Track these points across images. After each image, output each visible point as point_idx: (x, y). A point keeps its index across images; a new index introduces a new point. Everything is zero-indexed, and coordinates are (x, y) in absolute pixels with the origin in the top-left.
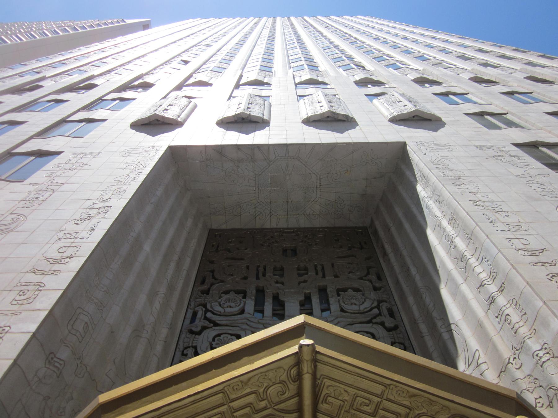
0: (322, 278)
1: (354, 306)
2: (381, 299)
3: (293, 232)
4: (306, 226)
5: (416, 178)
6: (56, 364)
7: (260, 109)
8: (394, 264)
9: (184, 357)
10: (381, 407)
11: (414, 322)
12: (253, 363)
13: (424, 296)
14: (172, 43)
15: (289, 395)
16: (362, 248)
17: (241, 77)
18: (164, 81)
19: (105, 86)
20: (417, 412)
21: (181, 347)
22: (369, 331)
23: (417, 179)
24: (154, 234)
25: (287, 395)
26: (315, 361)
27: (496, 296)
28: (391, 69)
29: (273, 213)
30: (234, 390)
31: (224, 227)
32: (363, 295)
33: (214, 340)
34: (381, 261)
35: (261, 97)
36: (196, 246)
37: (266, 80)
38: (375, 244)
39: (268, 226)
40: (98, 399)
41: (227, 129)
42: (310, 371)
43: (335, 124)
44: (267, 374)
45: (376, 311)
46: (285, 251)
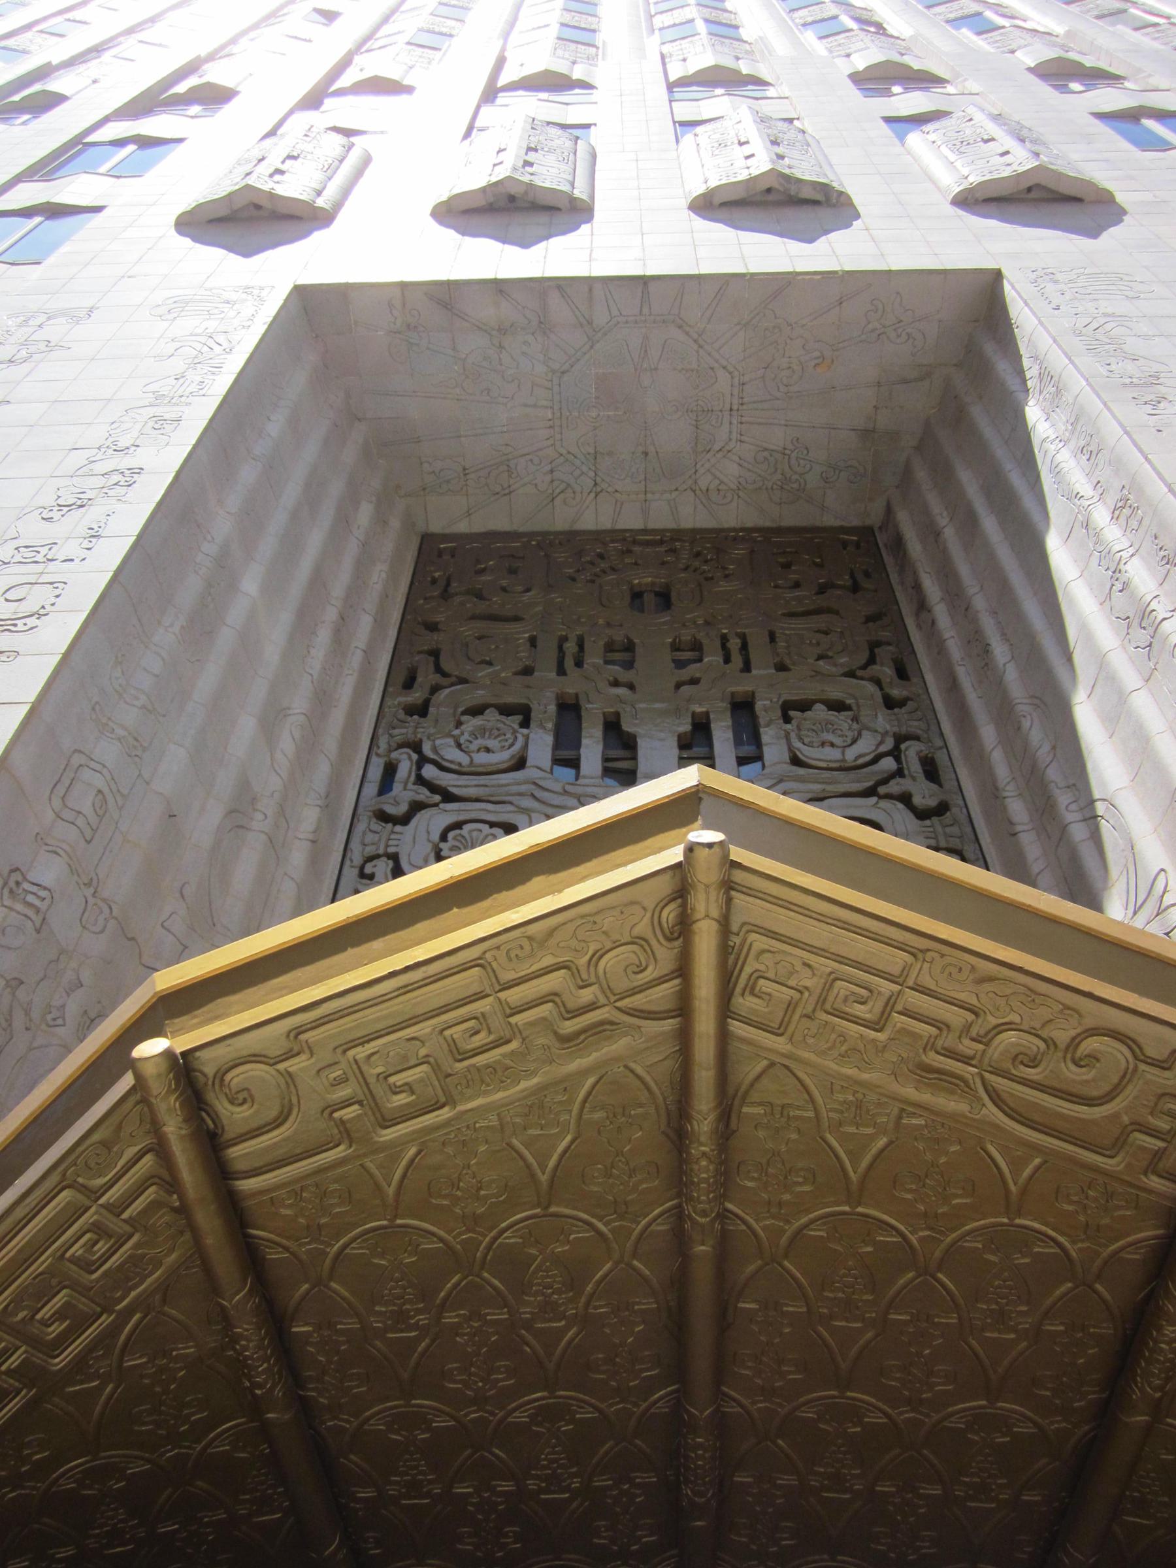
0: (742, 671)
1: (828, 749)
2: (904, 730)
3: (661, 542)
4: (698, 525)
5: (1024, 381)
6: (30, 898)
7: (563, 167)
8: (946, 635)
9: (365, 881)
10: (899, 1007)
11: (993, 795)
12: (560, 891)
13: (1026, 724)
14: (256, 26)
15: (656, 974)
16: (855, 588)
17: (500, 62)
18: (263, 80)
19: (90, 96)
20: (994, 1021)
21: (357, 857)
22: (868, 816)
23: (1029, 384)
24: (268, 546)
25: (650, 974)
26: (728, 886)
28: (966, 33)
29: (604, 486)
30: (510, 960)
31: (462, 527)
32: (855, 719)
33: (444, 837)
34: (910, 623)
35: (564, 127)
36: (386, 582)
37: (577, 74)
38: (894, 578)
39: (588, 523)
40: (154, 982)
41: (464, 234)
42: (715, 913)
43: (790, 212)
44: (597, 919)
45: (888, 764)
46: (637, 596)
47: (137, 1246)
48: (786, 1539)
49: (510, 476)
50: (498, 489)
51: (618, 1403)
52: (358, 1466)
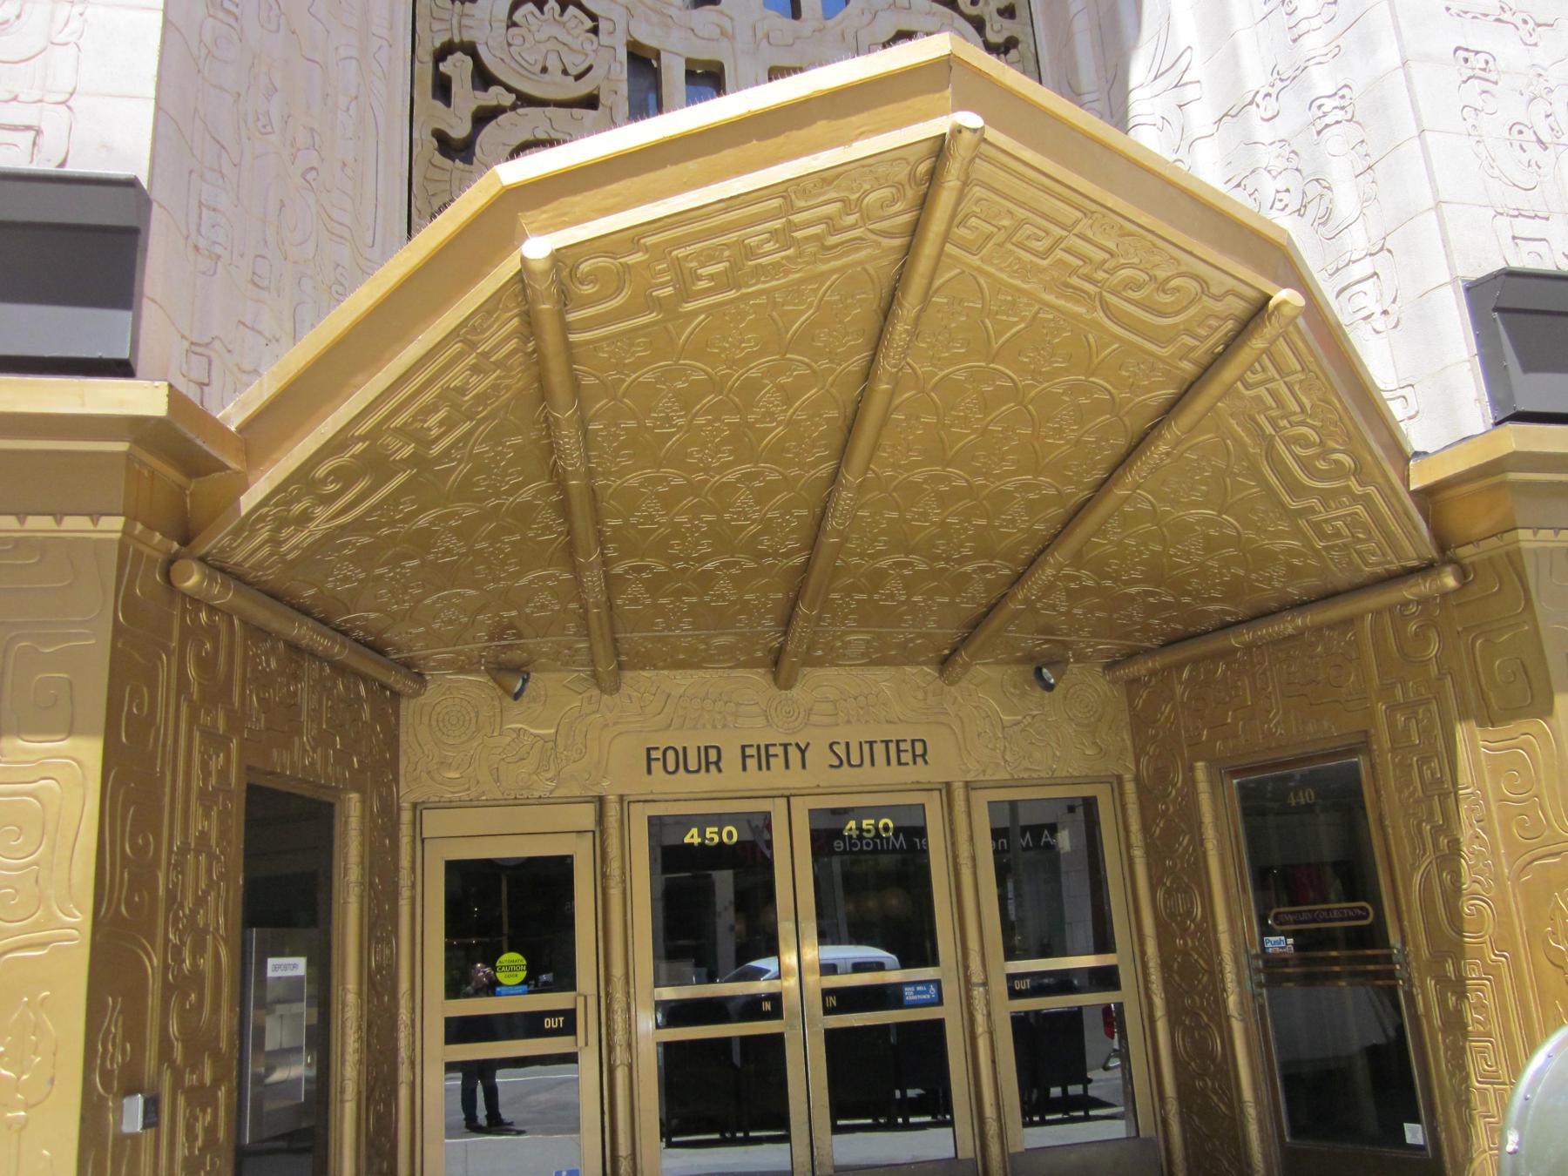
47: (498, 377)
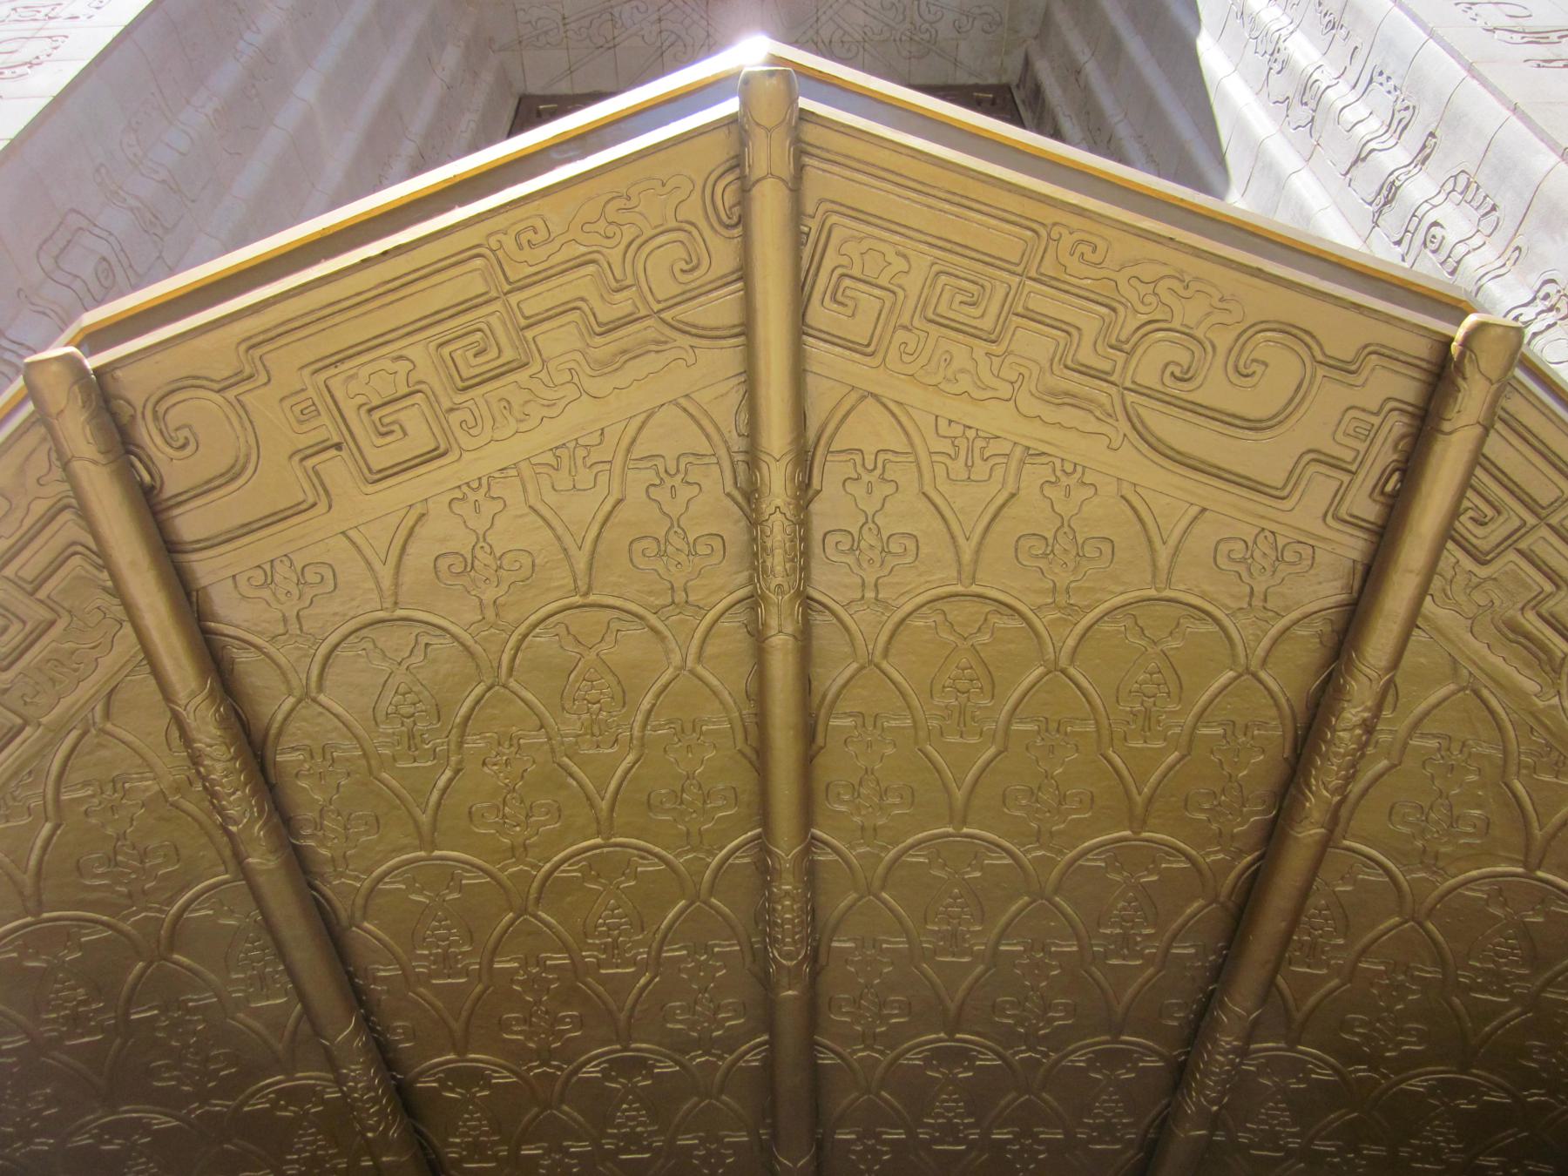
27: (1403, 178)
30: (521, 248)
48: (896, 1016)
49: (614, 27)
50: (601, 41)
51: (688, 852)
52: (379, 940)
